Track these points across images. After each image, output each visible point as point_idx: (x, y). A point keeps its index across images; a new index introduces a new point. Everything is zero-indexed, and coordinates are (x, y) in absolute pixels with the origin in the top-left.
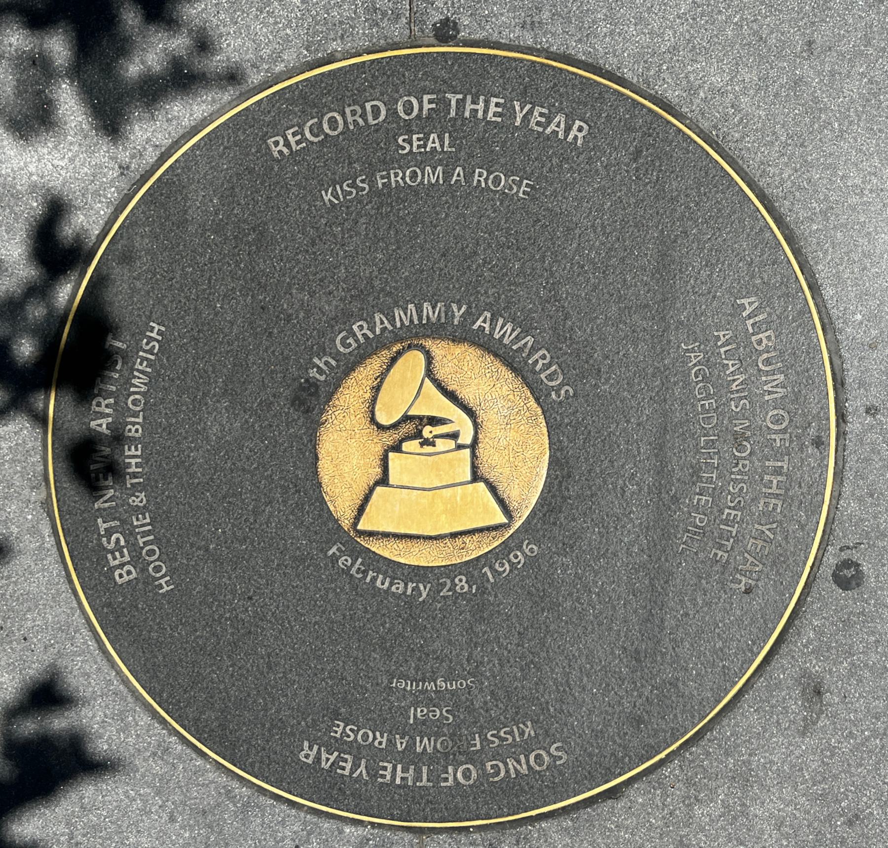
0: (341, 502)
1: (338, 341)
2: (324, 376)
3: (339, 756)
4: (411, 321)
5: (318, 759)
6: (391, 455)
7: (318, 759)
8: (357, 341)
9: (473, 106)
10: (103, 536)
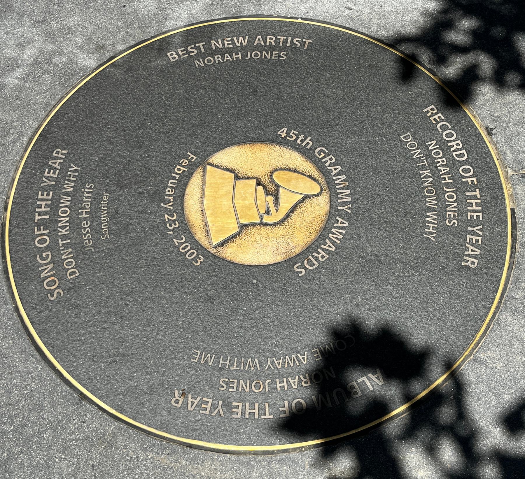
0: (230, 156)
3: (468, 244)
5: (475, 257)
6: (255, 180)
7: (475, 257)
8: (324, 157)
9: (474, 206)
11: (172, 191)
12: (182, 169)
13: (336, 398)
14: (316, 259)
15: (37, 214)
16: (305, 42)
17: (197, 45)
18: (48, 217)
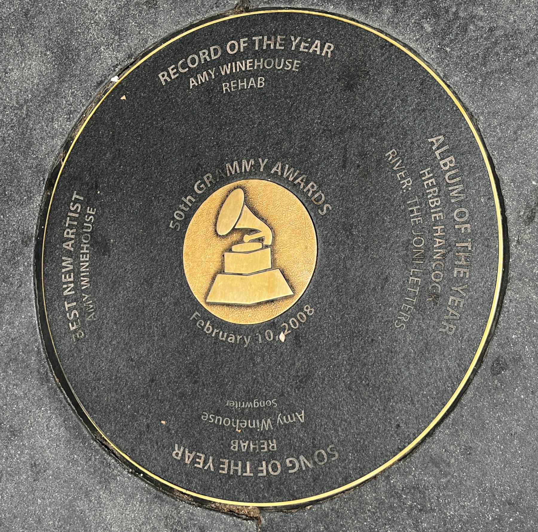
1: (196, 187)
2: (188, 208)
4: (236, 172)
6: (226, 254)
10: (72, 201)
11: (232, 336)
12: (207, 325)
13: (455, 181)
14: (314, 193)
15: (244, 474)
16: (75, 198)
17: (73, 199)
18: (248, 464)
